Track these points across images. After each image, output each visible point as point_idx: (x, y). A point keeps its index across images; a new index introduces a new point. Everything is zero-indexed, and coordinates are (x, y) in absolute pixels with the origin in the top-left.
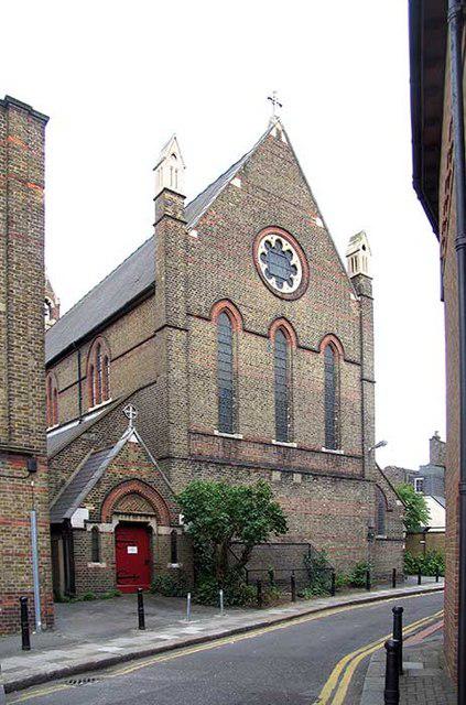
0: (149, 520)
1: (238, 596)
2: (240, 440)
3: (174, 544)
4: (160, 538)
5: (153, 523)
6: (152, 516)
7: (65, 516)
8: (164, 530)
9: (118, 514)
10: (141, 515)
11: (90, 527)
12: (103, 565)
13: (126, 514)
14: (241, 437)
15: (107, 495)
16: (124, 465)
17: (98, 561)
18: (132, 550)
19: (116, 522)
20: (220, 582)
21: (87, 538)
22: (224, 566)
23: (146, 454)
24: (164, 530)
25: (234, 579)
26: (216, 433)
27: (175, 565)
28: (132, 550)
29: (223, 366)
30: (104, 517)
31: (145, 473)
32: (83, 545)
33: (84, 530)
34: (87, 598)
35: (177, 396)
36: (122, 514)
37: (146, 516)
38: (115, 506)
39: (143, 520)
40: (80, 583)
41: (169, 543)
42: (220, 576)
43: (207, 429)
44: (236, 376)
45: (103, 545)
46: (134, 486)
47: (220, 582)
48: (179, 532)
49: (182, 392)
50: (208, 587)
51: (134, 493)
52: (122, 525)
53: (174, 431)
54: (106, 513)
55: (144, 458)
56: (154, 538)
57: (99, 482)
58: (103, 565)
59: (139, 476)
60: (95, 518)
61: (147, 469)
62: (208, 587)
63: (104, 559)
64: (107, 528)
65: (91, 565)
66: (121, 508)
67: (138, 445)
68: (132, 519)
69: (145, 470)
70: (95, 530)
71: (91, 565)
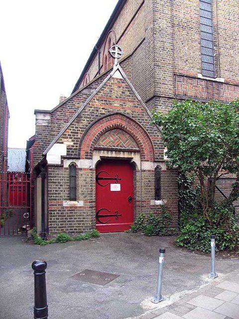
0: (133, 155)
1: (230, 240)
2: (222, 83)
3: (158, 180)
4: (143, 174)
5: (136, 159)
6: (135, 152)
7: (44, 153)
8: (148, 166)
9: (100, 149)
10: (124, 151)
11: (67, 163)
12: (80, 203)
13: (108, 150)
14: (222, 80)
15: (87, 131)
16: (107, 100)
17: (75, 199)
18: (115, 187)
19: (96, 158)
20: (207, 221)
21: (64, 174)
22: (211, 203)
23: (131, 91)
24: (148, 166)
25: (224, 219)
26: (200, 76)
27: (159, 202)
28: (115, 187)
29: (206, 59)
30: (83, 153)
31: (129, 108)
32: (59, 182)
33: (61, 166)
34: (60, 240)
35: (163, 41)
36: (104, 149)
37: (130, 151)
38: (97, 140)
39: (126, 155)
40: (55, 224)
41: (152, 178)
42: (208, 214)
43: (192, 72)
44: (215, 28)
45: (81, 182)
46: (116, 121)
47: (207, 221)
48: (163, 167)
49: (168, 40)
50: (193, 228)
51: (117, 128)
52: (103, 162)
53: (160, 74)
54: (85, 148)
55: (127, 93)
56: (138, 174)
57: (79, 116)
58: (80, 203)
59: (122, 111)
60: (73, 154)
61: (131, 104)
62: (193, 228)
63: (81, 197)
64: (87, 164)
65: (67, 204)
66: (102, 144)
67: (123, 80)
68: (114, 155)
69: (129, 105)
70: (73, 167)
71: (67, 204)
